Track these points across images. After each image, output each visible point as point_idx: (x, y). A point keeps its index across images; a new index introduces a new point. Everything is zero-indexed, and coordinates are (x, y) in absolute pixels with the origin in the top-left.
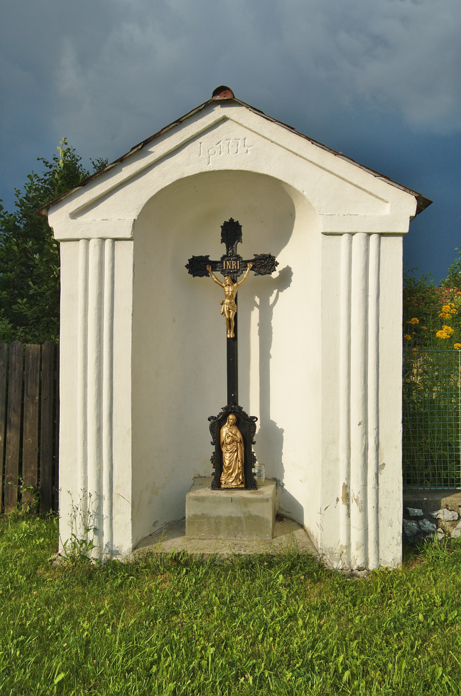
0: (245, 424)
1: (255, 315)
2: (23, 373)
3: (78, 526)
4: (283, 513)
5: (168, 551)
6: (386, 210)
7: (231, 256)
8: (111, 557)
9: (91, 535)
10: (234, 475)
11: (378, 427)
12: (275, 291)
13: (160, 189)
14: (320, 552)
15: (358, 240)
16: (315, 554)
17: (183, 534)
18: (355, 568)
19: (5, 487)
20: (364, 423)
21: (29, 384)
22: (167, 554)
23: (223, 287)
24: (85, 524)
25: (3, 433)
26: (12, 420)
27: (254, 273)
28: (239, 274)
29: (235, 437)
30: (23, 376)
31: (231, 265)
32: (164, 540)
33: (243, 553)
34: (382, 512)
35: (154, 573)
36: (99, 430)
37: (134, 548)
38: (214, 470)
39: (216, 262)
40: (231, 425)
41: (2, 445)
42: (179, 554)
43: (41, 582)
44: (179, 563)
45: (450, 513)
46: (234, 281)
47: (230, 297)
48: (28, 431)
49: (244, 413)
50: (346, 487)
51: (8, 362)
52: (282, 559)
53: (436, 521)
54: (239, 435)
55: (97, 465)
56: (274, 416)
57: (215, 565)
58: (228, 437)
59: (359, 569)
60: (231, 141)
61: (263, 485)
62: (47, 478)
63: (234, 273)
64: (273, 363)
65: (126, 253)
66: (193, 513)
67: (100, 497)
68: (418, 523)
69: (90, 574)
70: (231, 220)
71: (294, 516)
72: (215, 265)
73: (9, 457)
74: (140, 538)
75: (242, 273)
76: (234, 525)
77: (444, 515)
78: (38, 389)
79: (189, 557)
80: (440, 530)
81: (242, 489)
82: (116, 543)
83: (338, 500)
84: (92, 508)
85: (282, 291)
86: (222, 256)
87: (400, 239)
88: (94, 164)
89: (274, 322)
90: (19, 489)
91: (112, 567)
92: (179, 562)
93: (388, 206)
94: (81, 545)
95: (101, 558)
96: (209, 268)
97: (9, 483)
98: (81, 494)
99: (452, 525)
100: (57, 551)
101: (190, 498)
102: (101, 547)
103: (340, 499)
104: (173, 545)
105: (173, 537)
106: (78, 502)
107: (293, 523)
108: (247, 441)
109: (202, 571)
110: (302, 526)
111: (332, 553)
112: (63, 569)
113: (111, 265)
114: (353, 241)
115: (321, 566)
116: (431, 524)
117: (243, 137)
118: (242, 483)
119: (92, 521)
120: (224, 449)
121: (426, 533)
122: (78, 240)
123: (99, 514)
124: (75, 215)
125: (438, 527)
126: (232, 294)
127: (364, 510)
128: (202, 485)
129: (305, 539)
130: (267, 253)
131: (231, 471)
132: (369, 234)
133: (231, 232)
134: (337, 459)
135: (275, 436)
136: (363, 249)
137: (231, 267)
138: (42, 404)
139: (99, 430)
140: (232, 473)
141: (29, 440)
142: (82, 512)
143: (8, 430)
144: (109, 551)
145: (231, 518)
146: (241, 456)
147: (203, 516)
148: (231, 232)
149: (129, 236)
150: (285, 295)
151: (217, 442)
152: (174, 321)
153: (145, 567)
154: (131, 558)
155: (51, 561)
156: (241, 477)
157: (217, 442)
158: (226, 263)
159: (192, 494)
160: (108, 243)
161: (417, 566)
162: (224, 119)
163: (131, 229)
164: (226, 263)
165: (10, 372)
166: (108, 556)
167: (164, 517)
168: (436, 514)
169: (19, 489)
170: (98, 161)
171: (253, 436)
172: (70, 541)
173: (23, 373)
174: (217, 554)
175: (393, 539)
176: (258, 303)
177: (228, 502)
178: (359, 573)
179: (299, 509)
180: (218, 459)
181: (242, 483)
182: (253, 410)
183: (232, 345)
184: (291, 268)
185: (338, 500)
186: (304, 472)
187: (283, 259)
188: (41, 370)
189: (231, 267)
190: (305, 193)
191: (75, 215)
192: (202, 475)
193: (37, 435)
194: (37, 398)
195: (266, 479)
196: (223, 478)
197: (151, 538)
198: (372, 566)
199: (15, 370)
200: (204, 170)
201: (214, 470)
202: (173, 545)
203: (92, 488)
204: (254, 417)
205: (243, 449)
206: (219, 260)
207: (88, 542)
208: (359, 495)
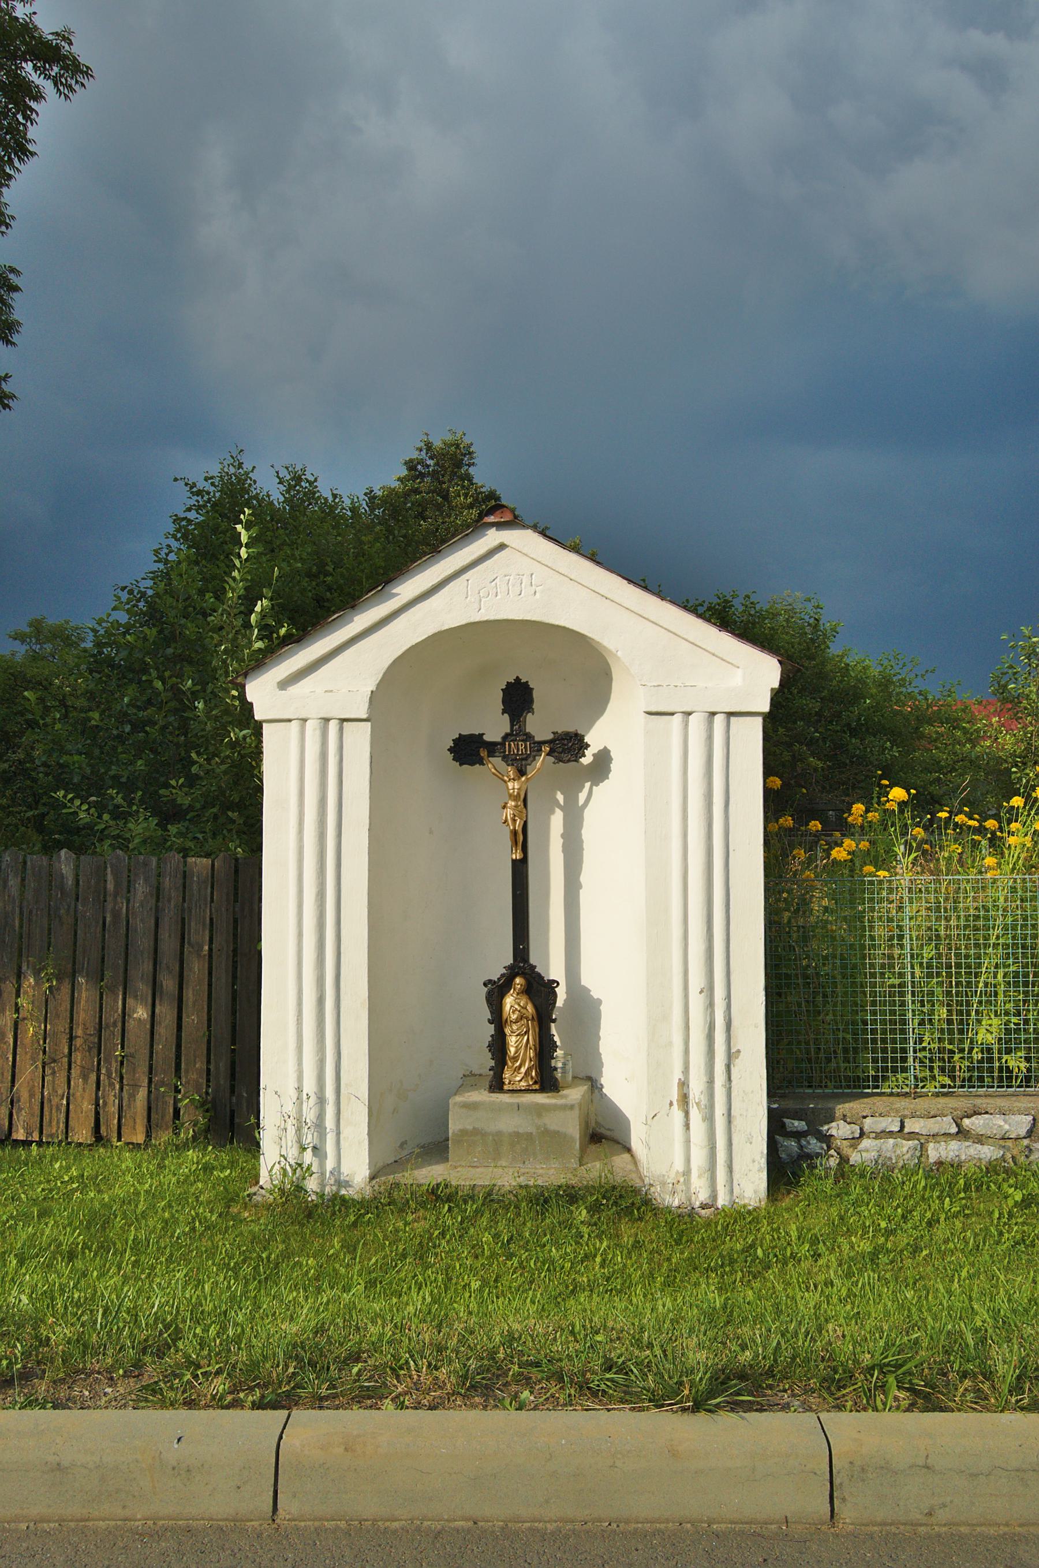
0: (540, 991)
1: (557, 821)
2: (182, 905)
3: (290, 1144)
4: (602, 1131)
5: (422, 1181)
6: (737, 679)
7: (517, 735)
8: (338, 1190)
9: (308, 1157)
10: (523, 1070)
11: (728, 997)
12: (588, 785)
13: (409, 646)
14: (647, 1181)
15: (696, 723)
16: (638, 1183)
17: (447, 1160)
18: (698, 1204)
19: (152, 1096)
20: (709, 990)
21: (193, 924)
22: (419, 1186)
23: (505, 782)
24: (299, 1141)
25: (150, 1008)
26: (164, 983)
27: (551, 759)
28: (529, 761)
29: (524, 1011)
30: (183, 910)
31: (520, 748)
32: (418, 1168)
33: (531, 1183)
34: (737, 1122)
35: (401, 1211)
36: (321, 1001)
37: (372, 1178)
38: (492, 1063)
39: (494, 744)
40: (518, 994)
41: (148, 1026)
42: (438, 1185)
43: (238, 1220)
44: (438, 1197)
45: (848, 1127)
46: (522, 772)
47: (516, 798)
48: (190, 1004)
49: (539, 975)
50: (683, 1084)
51: (158, 889)
52: (589, 1189)
53: (827, 1139)
54: (530, 1008)
55: (318, 1052)
56: (587, 979)
57: (491, 1200)
58: (513, 1012)
59: (703, 1206)
60: (512, 578)
61: (568, 1087)
62: (222, 1082)
63: (522, 759)
64: (585, 896)
65: (359, 741)
66: (461, 1127)
67: (321, 1101)
68: (799, 1142)
69: (310, 1212)
70: (518, 679)
71: (616, 1135)
72: (492, 748)
73: (159, 1047)
74: (380, 1164)
75: (534, 759)
76: (522, 1144)
77: (839, 1130)
78: (207, 932)
79: (453, 1189)
80: (832, 1152)
81: (535, 1091)
82: (345, 1169)
83: (671, 1104)
84: (310, 1114)
85: (597, 785)
86: (503, 734)
87: (759, 721)
88: (278, 477)
89: (586, 833)
90: (176, 1101)
91: (338, 1204)
92: (438, 1196)
93: (739, 672)
94: (294, 1171)
95: (323, 1191)
96: (483, 753)
97: (162, 1089)
98: (294, 1095)
99: (851, 1146)
100: (257, 1182)
101: (455, 1104)
102: (323, 1174)
103: (675, 1103)
104: (431, 1174)
105: (430, 1165)
106: (290, 1108)
107: (616, 1146)
108: (543, 1017)
109: (470, 1208)
110: (629, 1150)
111: (663, 1184)
112: (268, 1207)
113: (337, 757)
114: (690, 724)
115: (647, 1202)
116: (819, 1144)
117: (529, 573)
118: (535, 1083)
119: (310, 1136)
120: (507, 1031)
121: (809, 1157)
122: (290, 721)
123: (319, 1125)
124: (284, 684)
125: (829, 1148)
126: (518, 793)
127: (709, 1118)
128: (474, 1087)
129: (631, 1167)
130: (571, 729)
131: (518, 1064)
132: (713, 714)
133: (518, 698)
134: (670, 1044)
135: (587, 1010)
136: (703, 735)
137: (518, 750)
138: (215, 957)
139: (321, 1001)
140: (520, 1067)
141: (193, 1019)
142: (294, 1122)
143: (157, 1002)
144: (336, 1181)
145: (517, 1134)
146: (534, 1040)
147: (476, 1132)
148: (518, 698)
149: (365, 716)
150: (602, 791)
151: (498, 1020)
152: (431, 832)
153: (389, 1204)
154: (368, 1193)
155: (248, 1195)
156: (534, 1074)
157: (498, 1020)
158: (510, 745)
159: (458, 1099)
160: (333, 726)
161: (787, 1202)
162: (502, 547)
163: (367, 705)
164: (510, 745)
165: (160, 904)
166: (334, 1188)
167: (417, 1133)
168: (826, 1127)
169: (176, 1101)
170: (287, 468)
171: (552, 1010)
172: (277, 1166)
173: (182, 905)
174: (494, 1185)
175: (754, 1161)
176: (562, 803)
177: (511, 1112)
178: (703, 1212)
179: (621, 1121)
180: (498, 1046)
181: (535, 1083)
182: (555, 970)
183: (520, 871)
184: (609, 751)
185: (671, 1104)
186: (630, 1067)
187: (595, 739)
188: (212, 901)
189: (517, 750)
190: (619, 654)
191: (284, 684)
192: (476, 1071)
193: (206, 1010)
194: (206, 948)
195: (574, 1078)
196: (507, 1075)
197: (398, 1165)
198: (721, 1202)
199: (169, 901)
200: (472, 620)
201: (492, 1063)
202: (431, 1174)
203: (309, 1086)
204: (554, 981)
205: (537, 1030)
206: (499, 740)
207: (305, 1166)
208: (702, 1097)
